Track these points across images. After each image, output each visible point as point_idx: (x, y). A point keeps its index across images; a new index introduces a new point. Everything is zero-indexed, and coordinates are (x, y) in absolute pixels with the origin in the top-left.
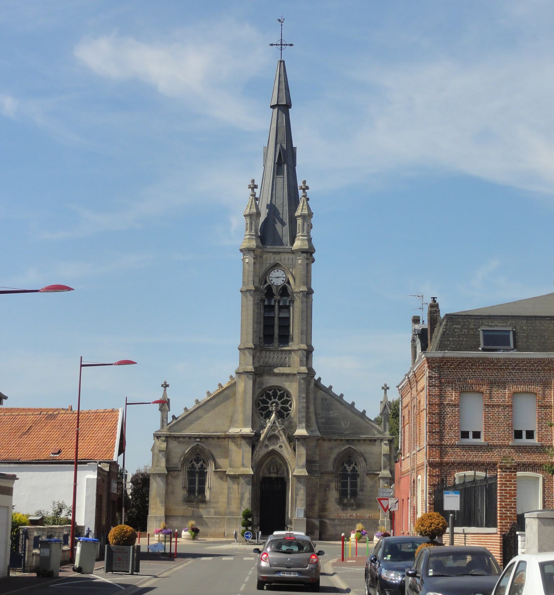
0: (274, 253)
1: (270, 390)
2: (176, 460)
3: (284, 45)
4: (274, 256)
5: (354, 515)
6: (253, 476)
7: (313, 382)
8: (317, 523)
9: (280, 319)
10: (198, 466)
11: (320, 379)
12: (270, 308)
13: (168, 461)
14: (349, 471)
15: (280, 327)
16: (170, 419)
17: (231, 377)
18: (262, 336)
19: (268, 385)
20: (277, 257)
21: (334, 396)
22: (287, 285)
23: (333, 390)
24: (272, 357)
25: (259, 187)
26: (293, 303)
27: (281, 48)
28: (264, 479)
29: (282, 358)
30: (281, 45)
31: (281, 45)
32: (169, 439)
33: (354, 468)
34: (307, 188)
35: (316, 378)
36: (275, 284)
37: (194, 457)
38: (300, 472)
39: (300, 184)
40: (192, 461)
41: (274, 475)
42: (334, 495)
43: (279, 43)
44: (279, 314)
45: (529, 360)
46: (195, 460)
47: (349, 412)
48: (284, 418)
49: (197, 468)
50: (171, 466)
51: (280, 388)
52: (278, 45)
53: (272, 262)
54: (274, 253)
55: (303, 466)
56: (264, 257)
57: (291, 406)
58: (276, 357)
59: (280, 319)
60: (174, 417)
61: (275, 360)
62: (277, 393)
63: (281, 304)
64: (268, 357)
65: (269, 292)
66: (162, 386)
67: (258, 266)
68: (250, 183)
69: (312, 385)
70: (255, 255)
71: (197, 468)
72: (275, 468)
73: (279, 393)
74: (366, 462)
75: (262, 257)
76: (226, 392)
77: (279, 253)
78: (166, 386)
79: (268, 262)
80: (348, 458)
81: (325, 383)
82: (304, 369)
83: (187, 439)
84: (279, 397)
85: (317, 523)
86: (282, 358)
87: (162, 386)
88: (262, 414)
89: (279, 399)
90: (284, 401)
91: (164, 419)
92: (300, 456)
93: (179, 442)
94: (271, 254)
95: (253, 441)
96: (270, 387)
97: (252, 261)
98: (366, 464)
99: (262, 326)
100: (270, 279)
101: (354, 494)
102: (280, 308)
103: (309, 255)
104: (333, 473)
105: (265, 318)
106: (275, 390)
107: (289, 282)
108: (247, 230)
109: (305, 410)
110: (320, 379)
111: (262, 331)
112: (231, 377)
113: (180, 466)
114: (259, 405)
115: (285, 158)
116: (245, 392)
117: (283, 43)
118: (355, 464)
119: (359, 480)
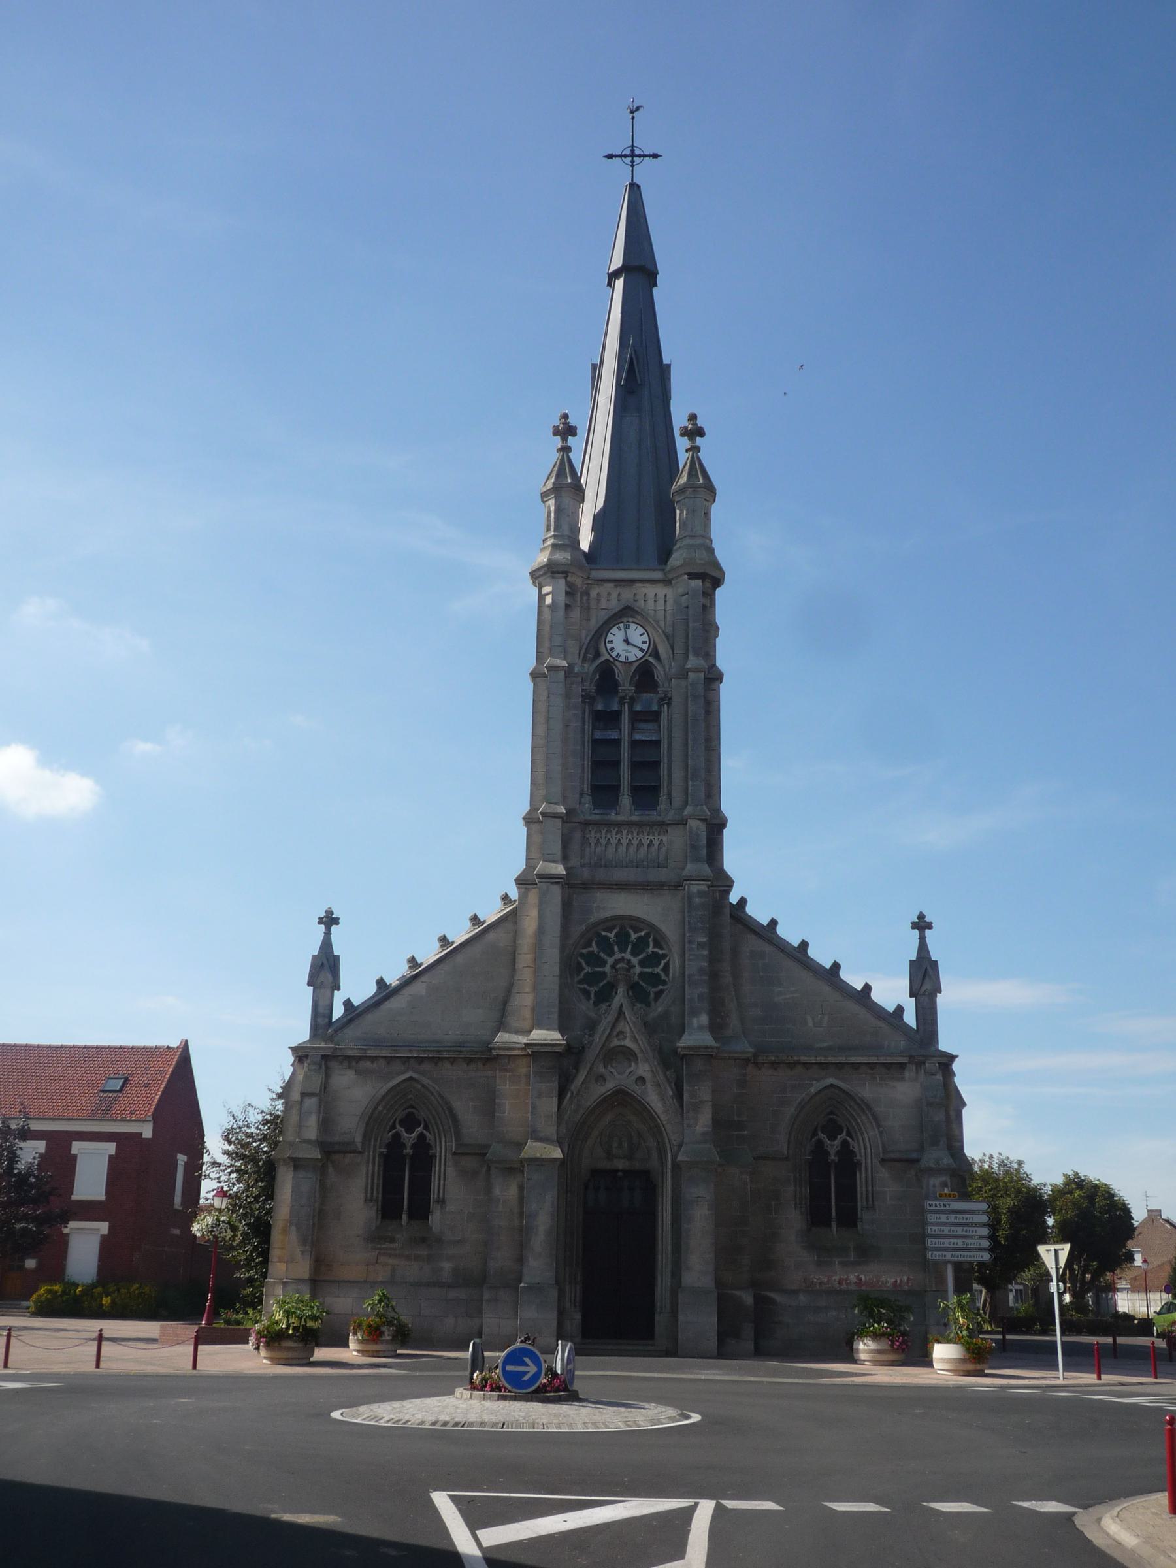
0: (618, 582)
1: (609, 930)
2: (350, 1124)
3: (639, 156)
4: (619, 589)
5: (852, 1278)
6: (562, 1162)
7: (727, 911)
8: (748, 1298)
9: (634, 744)
10: (409, 1138)
11: (743, 902)
12: (609, 719)
13: (326, 1124)
14: (833, 1151)
15: (635, 766)
16: (338, 1012)
17: (506, 898)
18: (587, 788)
19: (604, 914)
20: (627, 594)
21: (781, 946)
22: (652, 660)
23: (781, 931)
24: (614, 841)
25: (582, 432)
26: (669, 704)
27: (632, 162)
28: (595, 1173)
29: (640, 844)
30: (633, 155)
31: (633, 155)
32: (333, 1064)
33: (845, 1144)
34: (700, 432)
35: (734, 898)
36: (622, 659)
37: (400, 1114)
38: (915, 1376)
39: (679, 420)
40: (393, 1127)
41: (620, 1164)
42: (793, 1219)
43: (628, 152)
44: (631, 734)
45: (409, 1194)
46: (402, 1122)
47: (826, 989)
48: (648, 1005)
49: (409, 1144)
50: (336, 1139)
51: (636, 923)
52: (625, 156)
53: (614, 605)
54: (618, 582)
55: (704, 1134)
56: (594, 593)
57: (666, 969)
58: (625, 842)
59: (634, 744)
60: (348, 1004)
61: (622, 849)
62: (629, 936)
63: (638, 708)
64: (603, 842)
65: (606, 676)
66: (321, 921)
67: (576, 614)
68: (557, 422)
69: (726, 918)
70: (568, 584)
71: (409, 1144)
72: (625, 1145)
73: (634, 936)
74: (879, 1126)
75: (588, 594)
76: (491, 936)
77: (632, 582)
78: (329, 920)
79: (604, 604)
80: (832, 1118)
81: (759, 912)
82: (706, 870)
83: (382, 1062)
84: (635, 946)
85: (748, 1298)
86: (640, 844)
87: (321, 921)
88: (587, 993)
89: (634, 953)
90: (651, 974)
91: (321, 1013)
92: (696, 1107)
93: (359, 1073)
94: (612, 585)
95: (560, 1065)
96: (612, 918)
97: (562, 597)
98: (881, 1133)
99: (587, 763)
100: (609, 646)
101: (849, 1219)
102: (636, 717)
103: (708, 584)
104: (787, 1159)
105: (595, 743)
106: (623, 928)
107: (656, 654)
108: (548, 529)
109: (705, 978)
110: (743, 902)
111: (587, 775)
112: (506, 898)
113: (358, 1139)
114: (580, 968)
115: (643, 377)
116: (541, 931)
117: (637, 152)
118: (849, 1134)
119: (860, 1178)
